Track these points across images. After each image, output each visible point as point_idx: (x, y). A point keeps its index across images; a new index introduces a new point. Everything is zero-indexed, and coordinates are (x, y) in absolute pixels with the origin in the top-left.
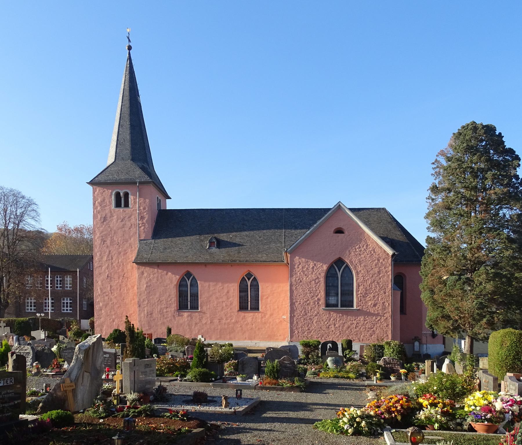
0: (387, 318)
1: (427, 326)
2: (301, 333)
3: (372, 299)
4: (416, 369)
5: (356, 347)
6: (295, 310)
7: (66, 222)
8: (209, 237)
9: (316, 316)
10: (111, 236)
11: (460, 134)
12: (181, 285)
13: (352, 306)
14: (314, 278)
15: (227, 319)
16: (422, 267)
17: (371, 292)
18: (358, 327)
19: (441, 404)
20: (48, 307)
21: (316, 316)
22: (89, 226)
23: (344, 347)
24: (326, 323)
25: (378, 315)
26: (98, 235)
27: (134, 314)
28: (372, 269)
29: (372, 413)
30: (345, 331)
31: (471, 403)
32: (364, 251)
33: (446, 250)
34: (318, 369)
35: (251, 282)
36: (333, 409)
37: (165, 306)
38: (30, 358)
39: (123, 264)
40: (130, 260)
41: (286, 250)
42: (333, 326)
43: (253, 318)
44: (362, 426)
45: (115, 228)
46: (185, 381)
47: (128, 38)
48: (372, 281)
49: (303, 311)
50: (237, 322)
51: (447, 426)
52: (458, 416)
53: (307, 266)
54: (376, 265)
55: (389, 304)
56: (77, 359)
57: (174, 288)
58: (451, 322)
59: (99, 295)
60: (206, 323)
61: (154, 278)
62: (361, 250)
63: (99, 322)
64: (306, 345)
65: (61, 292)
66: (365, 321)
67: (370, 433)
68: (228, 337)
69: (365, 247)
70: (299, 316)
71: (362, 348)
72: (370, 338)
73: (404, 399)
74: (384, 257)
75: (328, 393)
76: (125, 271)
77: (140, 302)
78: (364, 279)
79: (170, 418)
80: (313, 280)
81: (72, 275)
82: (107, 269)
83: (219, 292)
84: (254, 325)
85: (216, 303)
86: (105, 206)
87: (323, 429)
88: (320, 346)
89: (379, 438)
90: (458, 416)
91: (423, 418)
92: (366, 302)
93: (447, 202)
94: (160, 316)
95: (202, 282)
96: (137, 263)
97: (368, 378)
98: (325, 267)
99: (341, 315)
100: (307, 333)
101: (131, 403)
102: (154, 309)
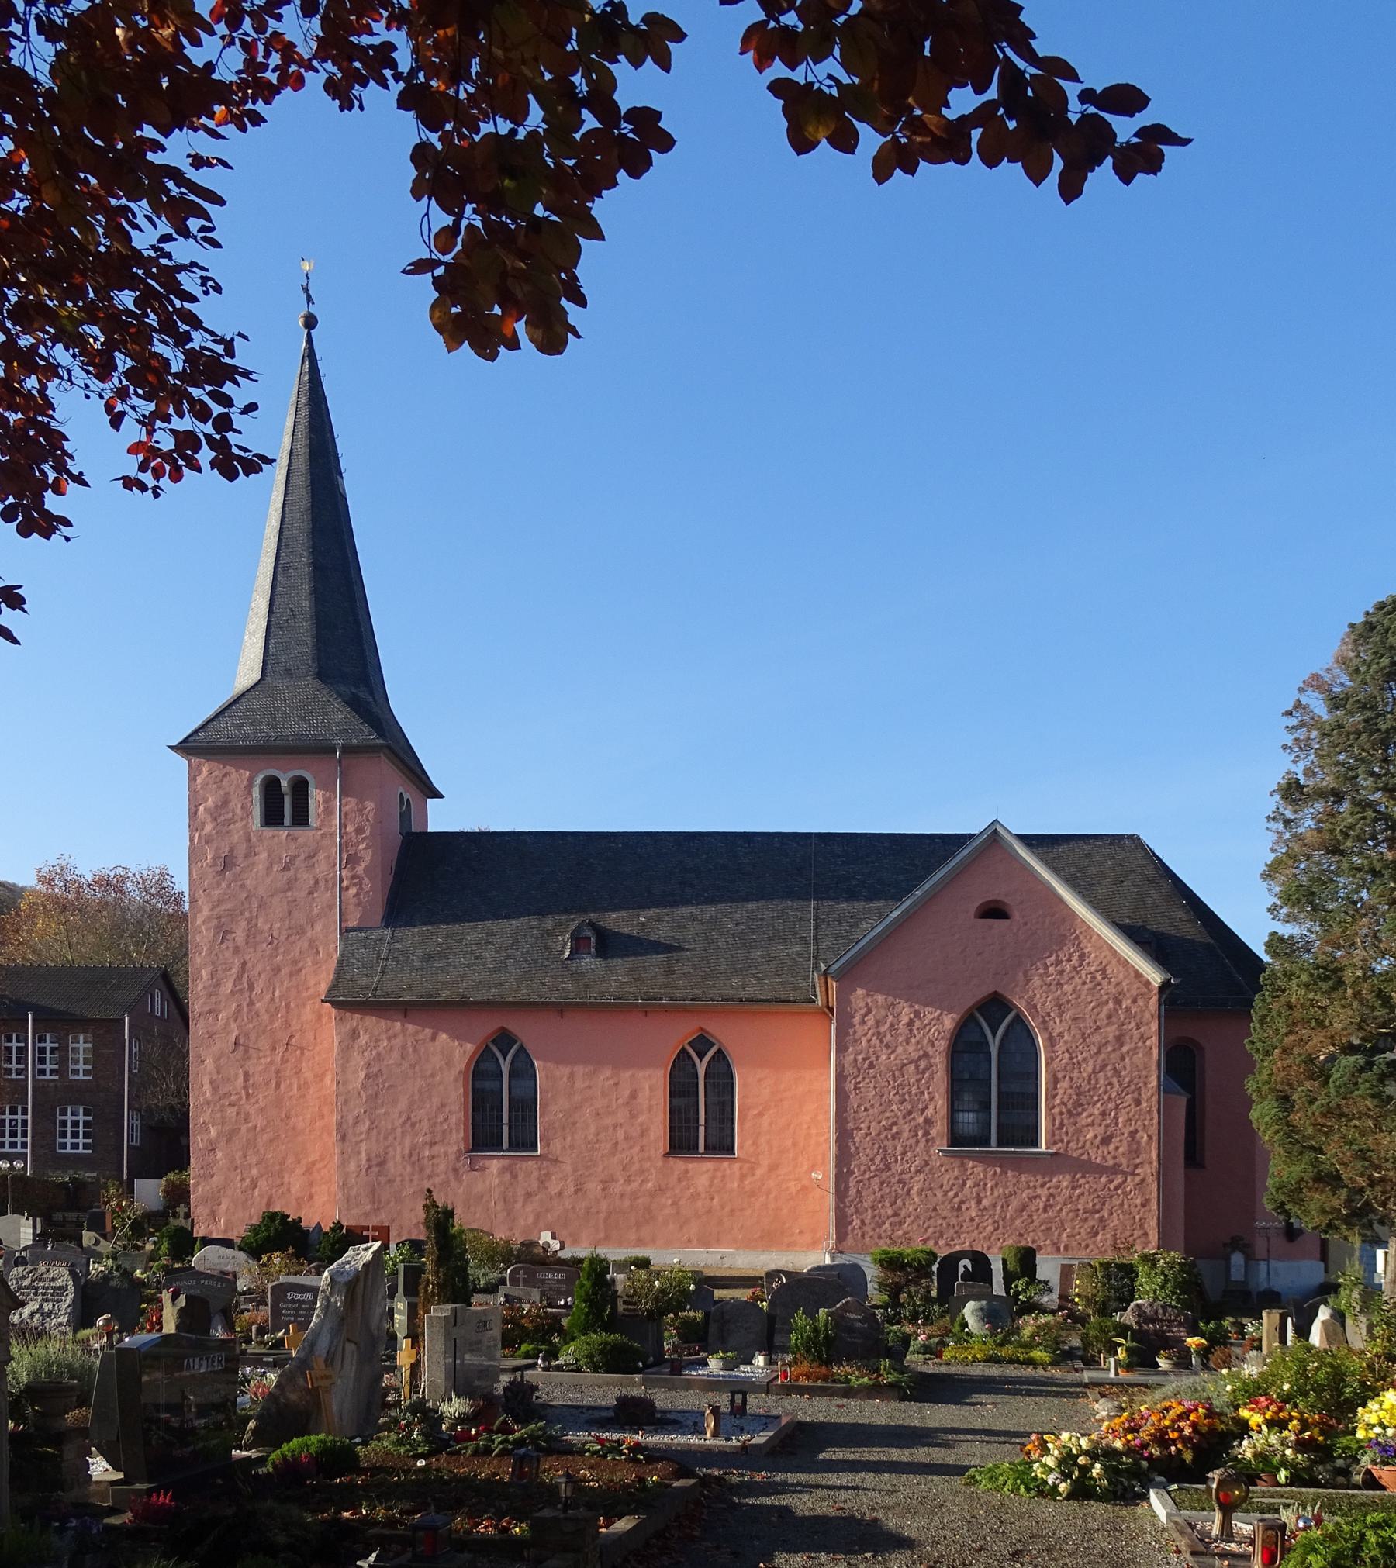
0: (1143, 1181)
1: (1269, 1207)
2: (873, 1225)
3: (1097, 1121)
4: (1233, 1336)
5: (1047, 1268)
6: (851, 1155)
7: (66, 856)
8: (574, 922)
9: (919, 1171)
10: (247, 914)
11: (1370, 627)
12: (481, 1074)
13: (1035, 1143)
14: (915, 1055)
15: (628, 1181)
16: (1255, 1024)
17: (1096, 1098)
18: (1051, 1206)
19: (1295, 1422)
20: (25, 1135)
21: (919, 1171)
22: (145, 873)
23: (1010, 1268)
24: (951, 1194)
25: (1115, 1170)
26: (206, 912)
27: (322, 1165)
28: (1098, 1028)
29: (1118, 1444)
30: (1013, 1219)
31: (1374, 1419)
32: (1074, 973)
33: (1326, 978)
34: (934, 1336)
35: (708, 1065)
36: (1005, 1443)
37: (428, 1138)
38: (68, 1302)
39: (287, 1006)
40: (311, 991)
41: (823, 967)
42: (973, 1204)
43: (712, 1179)
44: (1094, 1475)
45: (261, 892)
46: (559, 1368)
47: (306, 290)
48: (1098, 1067)
49: (879, 1158)
50: (661, 1190)
51: (1310, 1475)
52: (1340, 1451)
53: (890, 1018)
54: (1109, 1017)
55: (1150, 1137)
56: (327, 1308)
57: (456, 1080)
58: (1344, 1193)
59: (208, 1103)
60: (560, 1194)
61: (391, 1049)
62: (1062, 972)
63: (208, 1188)
64: (891, 1263)
65: (56, 1086)
66: (1074, 1188)
67: (1115, 1493)
68: (633, 1237)
69: (1075, 961)
70: (865, 1172)
71: (1066, 1272)
72: (1090, 1242)
73: (1200, 1410)
74: (1135, 992)
75: (981, 1404)
76: (295, 1025)
77: (345, 1126)
78: (1071, 1058)
79: (600, 1456)
80: (911, 1063)
81: (93, 1034)
82: (235, 1020)
83: (604, 1095)
84: (716, 1201)
85: (592, 1129)
86: (230, 822)
87: (990, 1486)
88: (935, 1268)
89: (1138, 1504)
90: (1340, 1451)
91: (1249, 1455)
92: (1079, 1131)
93: (1332, 831)
94: (409, 1168)
95: (549, 1064)
96: (336, 1004)
97: (1091, 1362)
98: (949, 1022)
99: (998, 1170)
100: (891, 1224)
101: (453, 1427)
102: (390, 1149)
